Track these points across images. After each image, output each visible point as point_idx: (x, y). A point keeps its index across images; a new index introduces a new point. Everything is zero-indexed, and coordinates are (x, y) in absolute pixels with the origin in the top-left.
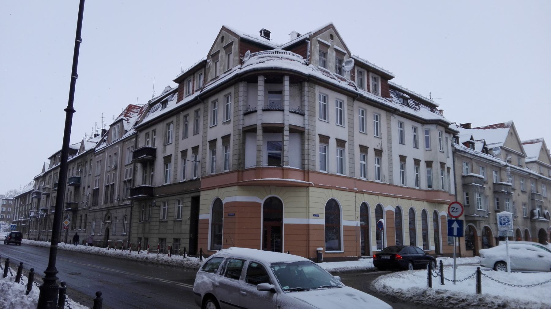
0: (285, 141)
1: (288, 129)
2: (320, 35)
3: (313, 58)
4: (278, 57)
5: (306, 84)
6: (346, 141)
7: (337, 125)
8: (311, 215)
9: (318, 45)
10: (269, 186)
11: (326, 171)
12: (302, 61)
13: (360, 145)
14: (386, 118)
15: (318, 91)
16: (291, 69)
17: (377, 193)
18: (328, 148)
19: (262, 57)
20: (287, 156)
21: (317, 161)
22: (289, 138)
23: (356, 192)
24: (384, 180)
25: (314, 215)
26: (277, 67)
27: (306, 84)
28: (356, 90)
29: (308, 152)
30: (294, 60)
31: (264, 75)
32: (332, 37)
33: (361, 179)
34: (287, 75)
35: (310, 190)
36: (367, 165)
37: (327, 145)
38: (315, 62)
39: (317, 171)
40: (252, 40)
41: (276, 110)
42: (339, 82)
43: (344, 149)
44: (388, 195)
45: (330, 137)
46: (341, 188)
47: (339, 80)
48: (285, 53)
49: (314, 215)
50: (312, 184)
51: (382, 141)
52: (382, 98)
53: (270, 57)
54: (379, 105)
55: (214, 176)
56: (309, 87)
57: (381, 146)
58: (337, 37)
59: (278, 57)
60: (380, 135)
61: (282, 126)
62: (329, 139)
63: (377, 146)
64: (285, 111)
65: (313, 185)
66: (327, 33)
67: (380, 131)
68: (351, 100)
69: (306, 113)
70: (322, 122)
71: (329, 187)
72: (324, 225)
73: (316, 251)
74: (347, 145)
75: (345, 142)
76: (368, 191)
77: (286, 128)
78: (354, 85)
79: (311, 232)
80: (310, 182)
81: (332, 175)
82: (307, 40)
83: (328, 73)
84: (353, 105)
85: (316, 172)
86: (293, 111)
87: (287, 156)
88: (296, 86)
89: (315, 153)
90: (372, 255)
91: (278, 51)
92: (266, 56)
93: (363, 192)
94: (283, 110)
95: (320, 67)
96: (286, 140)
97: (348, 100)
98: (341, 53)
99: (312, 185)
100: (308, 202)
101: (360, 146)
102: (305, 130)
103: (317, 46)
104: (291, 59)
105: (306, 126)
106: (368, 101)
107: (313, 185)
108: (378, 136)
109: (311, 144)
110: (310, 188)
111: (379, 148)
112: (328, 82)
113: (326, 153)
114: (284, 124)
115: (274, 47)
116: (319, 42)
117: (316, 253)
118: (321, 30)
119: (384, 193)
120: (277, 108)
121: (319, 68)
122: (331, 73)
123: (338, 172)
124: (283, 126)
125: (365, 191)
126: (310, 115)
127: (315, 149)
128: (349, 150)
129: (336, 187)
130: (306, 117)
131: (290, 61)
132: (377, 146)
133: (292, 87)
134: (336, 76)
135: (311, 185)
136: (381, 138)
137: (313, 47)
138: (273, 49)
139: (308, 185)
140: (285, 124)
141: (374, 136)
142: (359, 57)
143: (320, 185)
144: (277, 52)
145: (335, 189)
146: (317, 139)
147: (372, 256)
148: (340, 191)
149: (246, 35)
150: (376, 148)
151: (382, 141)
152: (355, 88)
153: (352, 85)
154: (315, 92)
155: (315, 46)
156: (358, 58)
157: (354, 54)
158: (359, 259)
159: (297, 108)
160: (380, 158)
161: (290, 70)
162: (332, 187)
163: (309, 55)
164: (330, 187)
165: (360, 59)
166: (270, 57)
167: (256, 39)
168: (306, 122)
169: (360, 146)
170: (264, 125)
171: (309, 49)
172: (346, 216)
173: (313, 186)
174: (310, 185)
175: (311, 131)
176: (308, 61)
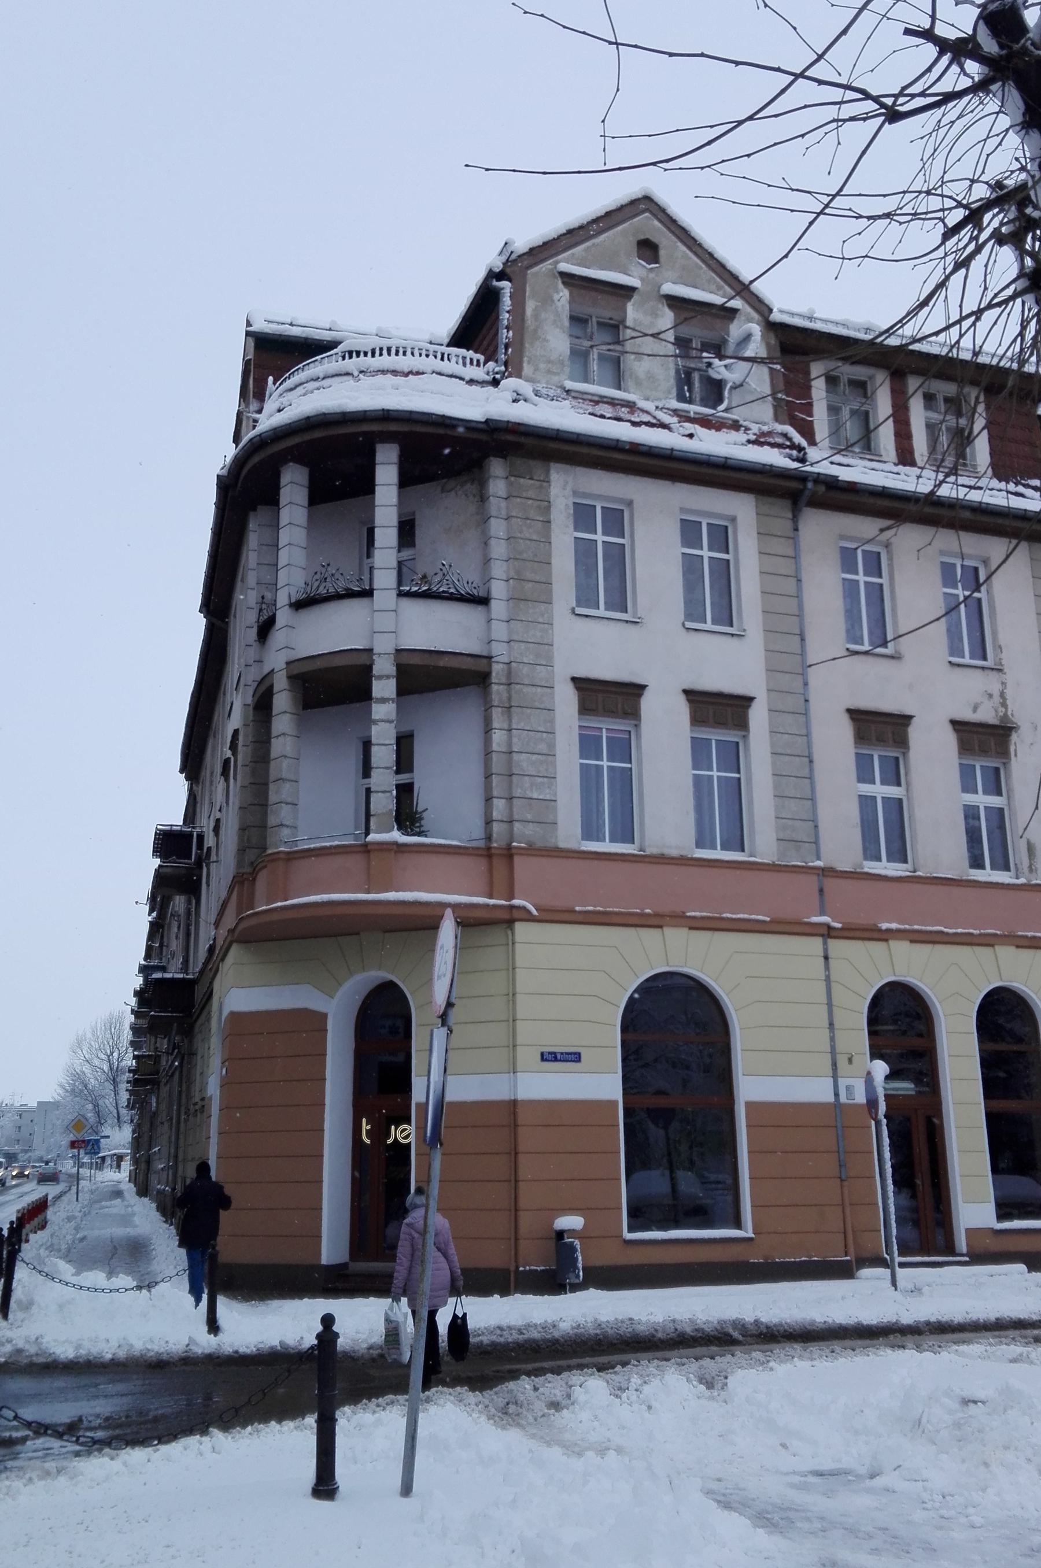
0: (375, 722)
1: (392, 670)
2: (578, 250)
3: (531, 350)
4: (347, 374)
5: (497, 468)
6: (751, 699)
7: (688, 629)
8: (528, 1056)
9: (563, 295)
10: (358, 934)
11: (743, 850)
12: (478, 373)
13: (850, 711)
14: (1029, 574)
15: (568, 491)
16: (388, 411)
17: (976, 932)
18: (639, 737)
19: (292, 386)
20: (384, 792)
21: (560, 804)
22: (399, 710)
23: (828, 933)
24: (1031, 869)
25: (550, 1057)
26: (324, 411)
27: (497, 468)
28: (803, 460)
29: (510, 763)
30: (418, 373)
31: (300, 456)
32: (648, 249)
33: (866, 870)
34: (388, 437)
35: (518, 938)
36: (1010, 809)
37: (904, 754)
38: (542, 366)
39: (562, 845)
40: (304, 335)
41: (338, 597)
42: (691, 436)
43: (1004, 764)
44: (971, 934)
45: (643, 687)
46: (723, 919)
47: (690, 428)
48: (385, 352)
49: (550, 1057)
50: (524, 908)
51: (1003, 684)
52: (995, 483)
53: (317, 379)
54: (967, 515)
55: (223, 914)
56: (512, 479)
57: (1004, 704)
58: (679, 244)
59: (347, 374)
60: (996, 656)
61: (363, 660)
62: (640, 695)
63: (975, 709)
64: (493, 603)
65: (535, 912)
66: (622, 235)
67: (994, 633)
68: (782, 510)
69: (498, 590)
70: (598, 620)
71: (643, 915)
72: (613, 1104)
73: (554, 1235)
74: (758, 716)
75: (747, 701)
76: (916, 927)
77: (384, 666)
78: (790, 439)
79: (527, 1140)
80: (516, 902)
81: (661, 859)
82: (499, 280)
83: (631, 406)
84: (796, 529)
85: (562, 850)
86: (414, 589)
87: (384, 792)
88: (468, 486)
89: (554, 764)
90: (964, 1250)
91: (475, 367)
92: (304, 380)
93: (880, 930)
94: (483, 601)
95: (569, 384)
96: (383, 721)
97: (757, 514)
98: (714, 311)
99: (529, 912)
100: (512, 996)
101: (857, 716)
102: (490, 666)
103: (556, 297)
104: (406, 370)
105: (499, 650)
106: (928, 510)
107: (535, 912)
108: (985, 658)
109: (521, 725)
110: (519, 927)
111: (987, 715)
112: (572, 433)
113: (739, 772)
114: (370, 651)
115: (338, 339)
116: (568, 279)
117: (552, 1243)
118: (581, 227)
119: (1030, 934)
120: (341, 586)
121: (568, 392)
122: (642, 404)
123: (977, 862)
124: (486, 669)
125: (894, 926)
126: (516, 599)
127: (552, 745)
128: (771, 737)
129: (688, 914)
130: (498, 608)
131: (400, 380)
132: (975, 709)
133: (453, 493)
134: (675, 412)
135: (523, 915)
136: (1000, 670)
137: (530, 306)
138: (332, 345)
139: (506, 916)
140: (375, 651)
141: (950, 662)
142: (815, 315)
143: (577, 908)
144: (350, 353)
145: (685, 926)
146: (566, 700)
147: (962, 1255)
148: (718, 935)
149: (278, 323)
150: (967, 715)
151: (1003, 684)
152: (794, 453)
153: (779, 440)
154: (548, 494)
155: (547, 301)
156: (811, 318)
157: (785, 308)
158: (858, 1269)
159: (440, 574)
160: (904, 754)
161: (386, 416)
162: (656, 915)
163: (505, 341)
164: (648, 915)
165: (825, 321)
166: (317, 379)
167: (330, 330)
168: (499, 630)
169: (857, 716)
170: (298, 669)
171: (507, 315)
172: (429, 1038)
173: (530, 918)
174: (516, 914)
175: (525, 670)
176: (503, 368)
